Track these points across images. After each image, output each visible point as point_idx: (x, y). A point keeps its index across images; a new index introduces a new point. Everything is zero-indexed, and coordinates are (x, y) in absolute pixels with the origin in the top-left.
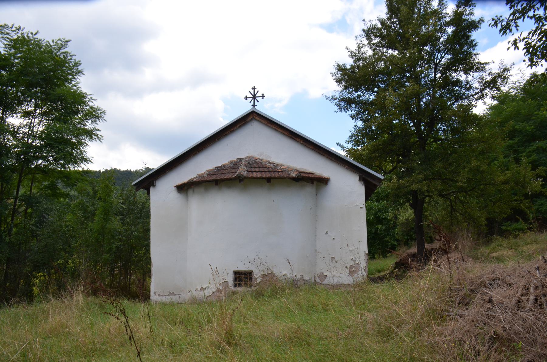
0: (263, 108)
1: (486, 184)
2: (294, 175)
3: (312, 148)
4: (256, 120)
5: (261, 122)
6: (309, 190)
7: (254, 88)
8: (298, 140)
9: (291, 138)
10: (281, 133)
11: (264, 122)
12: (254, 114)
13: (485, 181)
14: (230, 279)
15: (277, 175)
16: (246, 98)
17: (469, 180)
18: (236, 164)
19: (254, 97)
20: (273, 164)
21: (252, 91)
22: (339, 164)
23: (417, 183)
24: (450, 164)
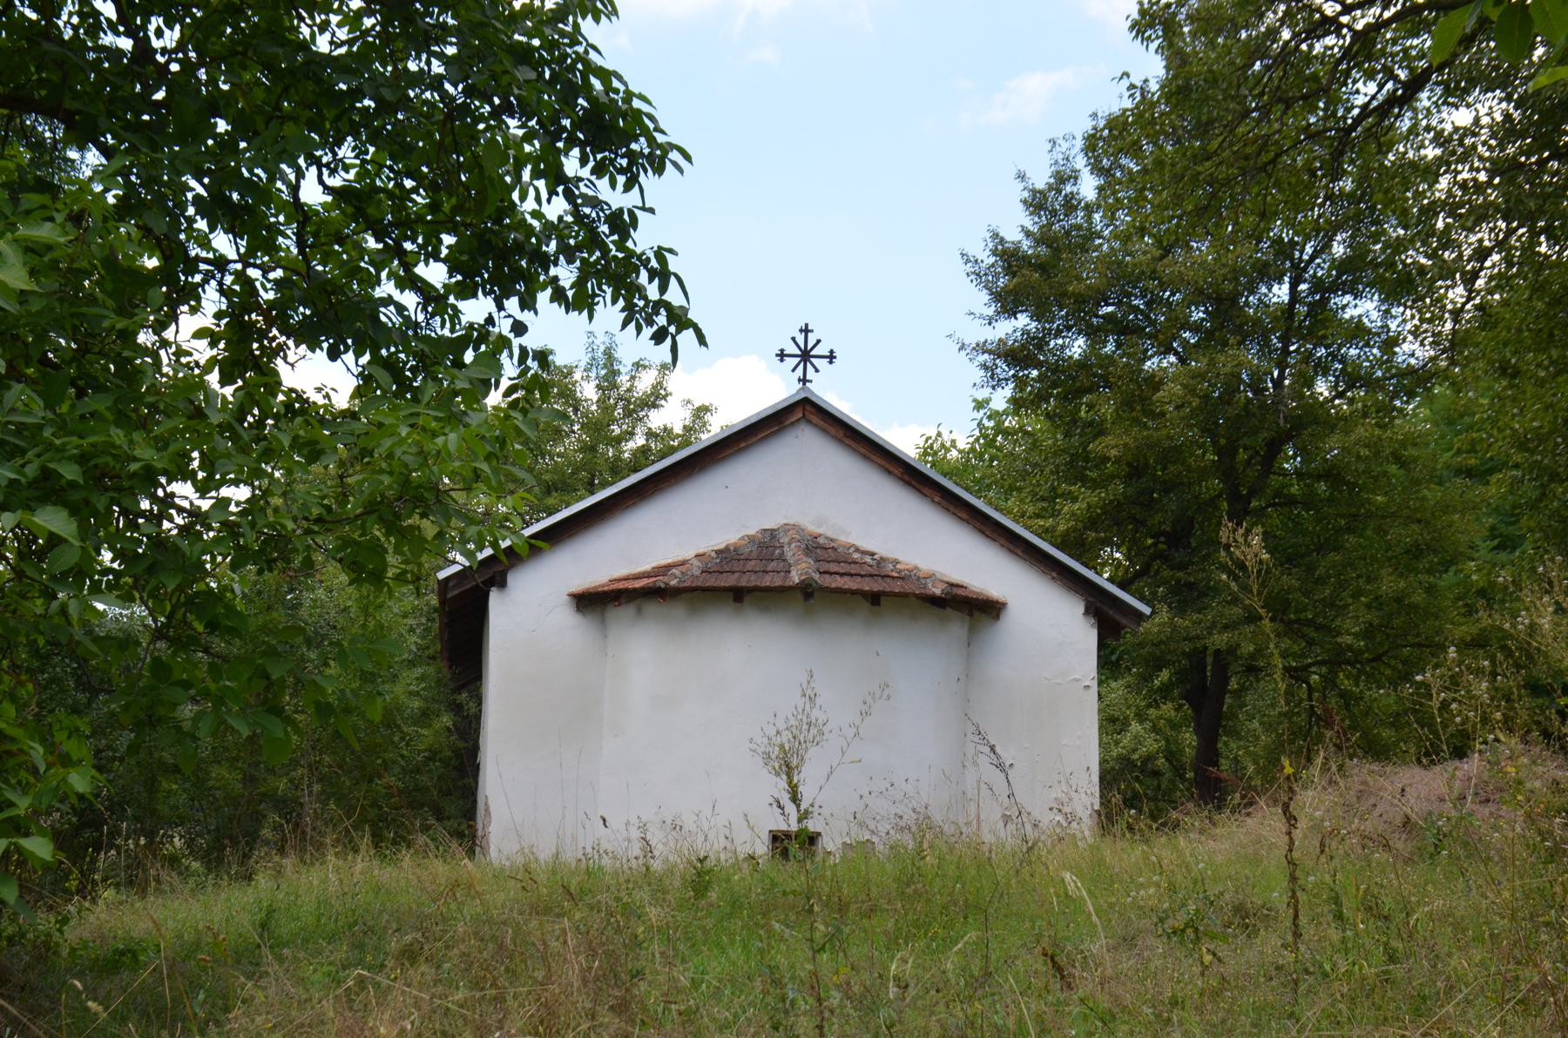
0: (830, 389)
1: (1420, 645)
2: (938, 592)
3: (965, 516)
4: (809, 422)
5: (824, 431)
6: (957, 628)
7: (806, 331)
8: (925, 490)
9: (908, 483)
10: (881, 466)
11: (833, 431)
12: (808, 407)
13: (1418, 635)
14: (762, 848)
15: (897, 587)
16: (782, 355)
17: (1368, 633)
18: (767, 545)
19: (806, 356)
20: (873, 554)
21: (800, 339)
22: (724, 458)
23: (1226, 628)
24: (1321, 581)
